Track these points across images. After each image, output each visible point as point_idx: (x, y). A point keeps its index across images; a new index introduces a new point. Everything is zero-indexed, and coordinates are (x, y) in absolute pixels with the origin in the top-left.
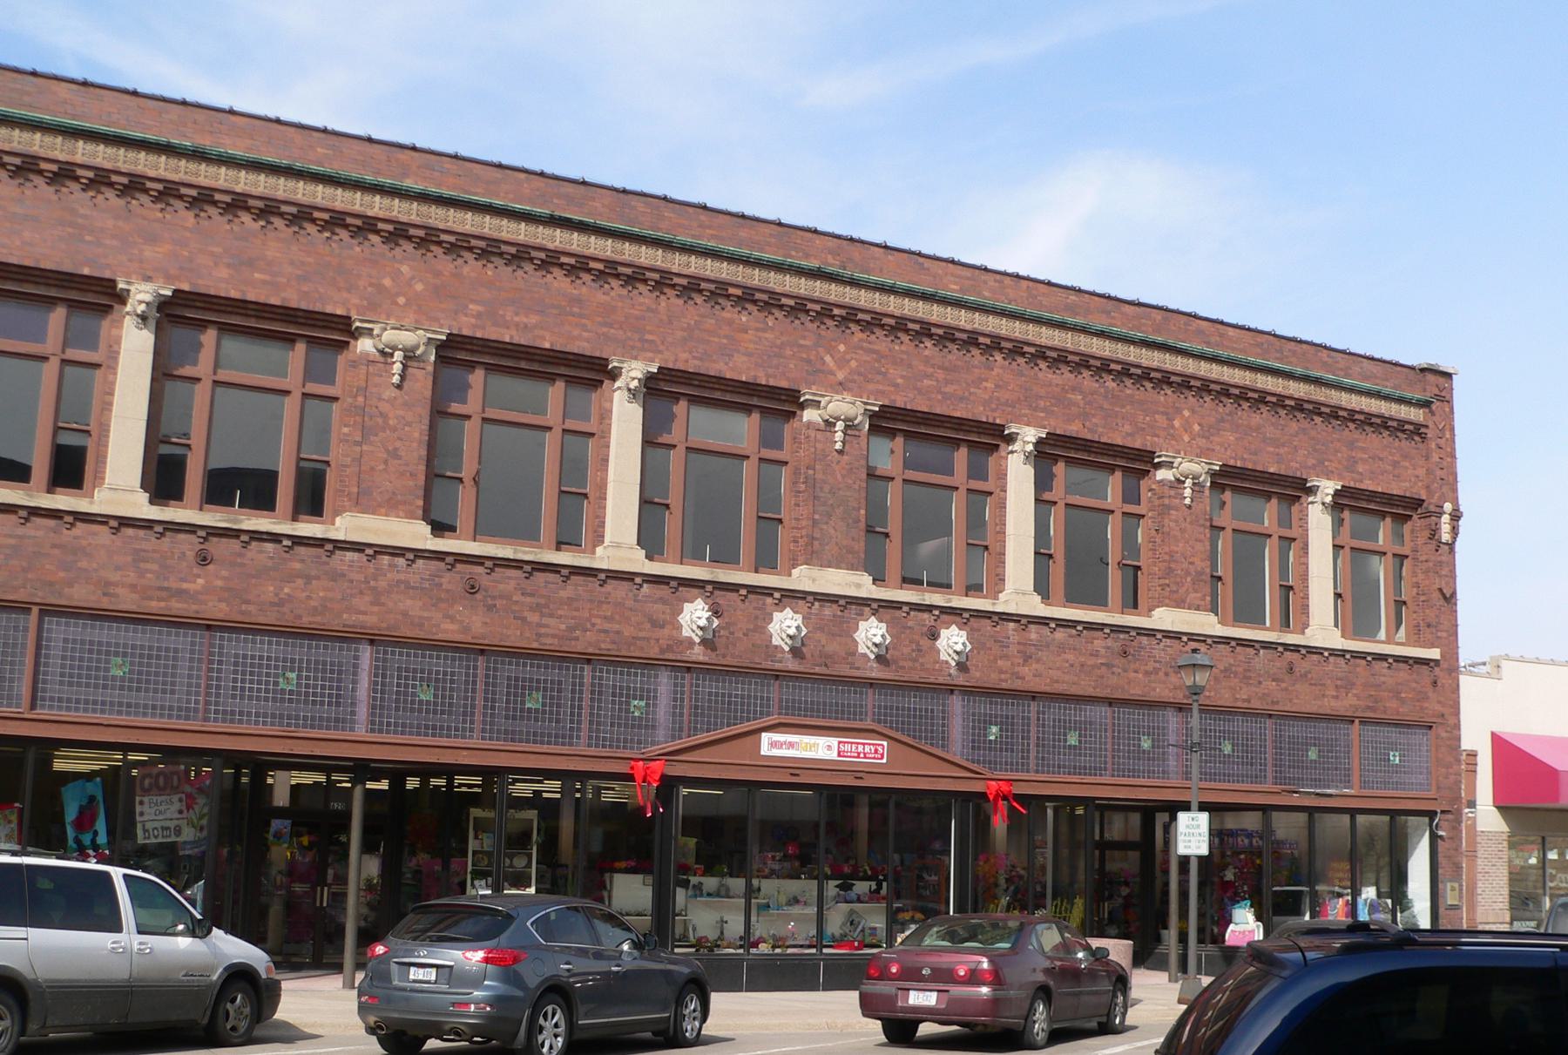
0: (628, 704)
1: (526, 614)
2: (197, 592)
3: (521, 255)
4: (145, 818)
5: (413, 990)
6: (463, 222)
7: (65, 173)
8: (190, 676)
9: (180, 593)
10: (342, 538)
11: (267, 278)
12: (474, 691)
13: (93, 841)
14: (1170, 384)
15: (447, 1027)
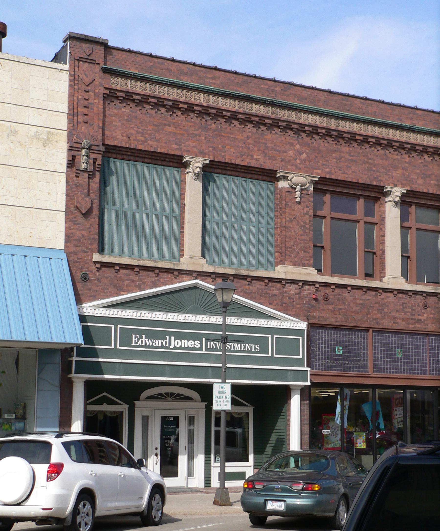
2: (424, 320)
4: (398, 416)
6: (126, 85)
9: (419, 321)
14: (416, 151)
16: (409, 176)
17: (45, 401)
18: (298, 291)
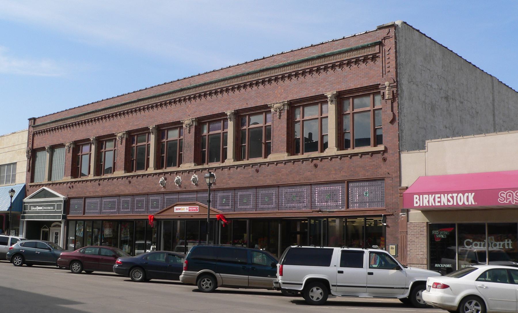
9: (97, 192)
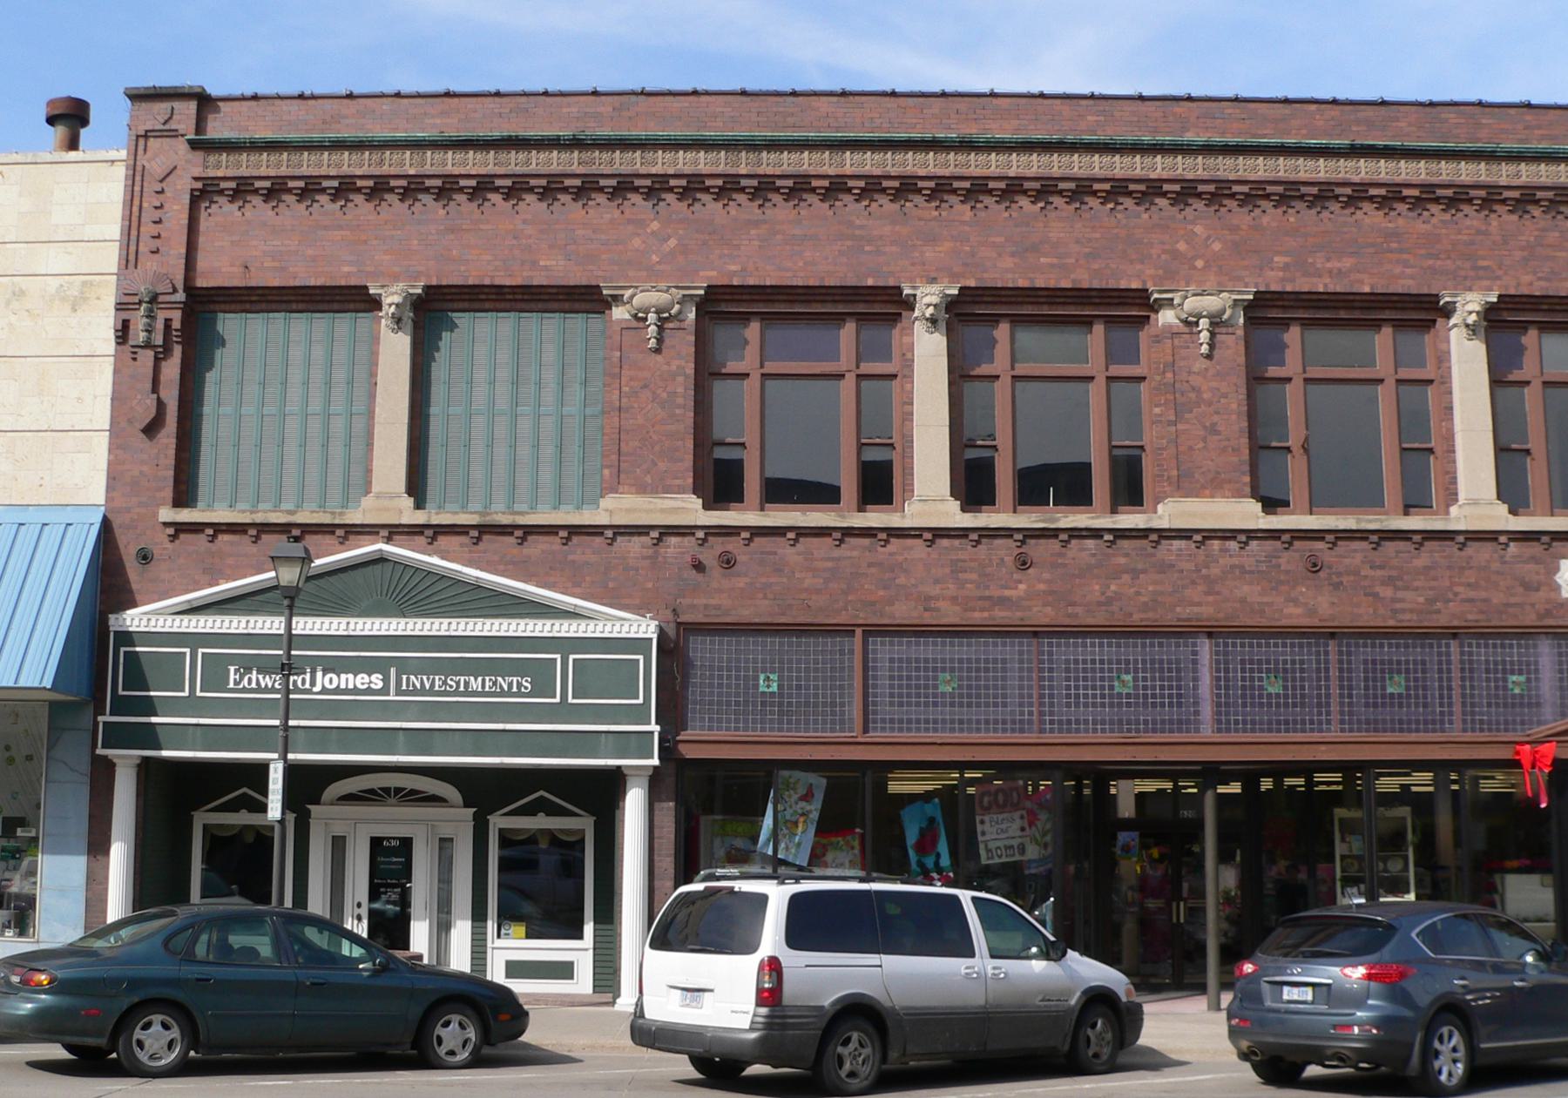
0: (1505, 680)
1: (1378, 589)
3: (1324, 194)
4: (987, 837)
5: (1287, 1012)
6: (1255, 169)
7: (836, 187)
8: (1021, 687)
9: (1003, 602)
10: (1166, 525)
11: (1055, 261)
12: (1327, 679)
13: (937, 864)
15: (1329, 1052)
16: (973, 255)
17: (64, 803)
18: (651, 551)
